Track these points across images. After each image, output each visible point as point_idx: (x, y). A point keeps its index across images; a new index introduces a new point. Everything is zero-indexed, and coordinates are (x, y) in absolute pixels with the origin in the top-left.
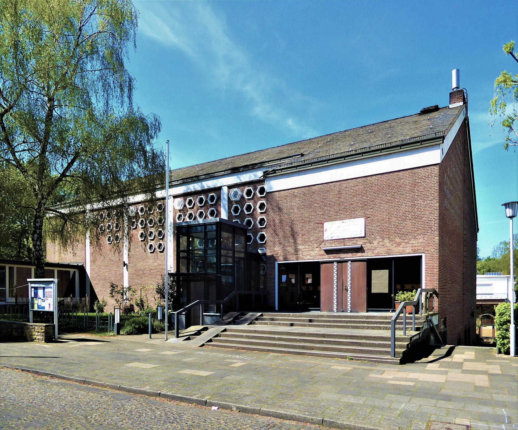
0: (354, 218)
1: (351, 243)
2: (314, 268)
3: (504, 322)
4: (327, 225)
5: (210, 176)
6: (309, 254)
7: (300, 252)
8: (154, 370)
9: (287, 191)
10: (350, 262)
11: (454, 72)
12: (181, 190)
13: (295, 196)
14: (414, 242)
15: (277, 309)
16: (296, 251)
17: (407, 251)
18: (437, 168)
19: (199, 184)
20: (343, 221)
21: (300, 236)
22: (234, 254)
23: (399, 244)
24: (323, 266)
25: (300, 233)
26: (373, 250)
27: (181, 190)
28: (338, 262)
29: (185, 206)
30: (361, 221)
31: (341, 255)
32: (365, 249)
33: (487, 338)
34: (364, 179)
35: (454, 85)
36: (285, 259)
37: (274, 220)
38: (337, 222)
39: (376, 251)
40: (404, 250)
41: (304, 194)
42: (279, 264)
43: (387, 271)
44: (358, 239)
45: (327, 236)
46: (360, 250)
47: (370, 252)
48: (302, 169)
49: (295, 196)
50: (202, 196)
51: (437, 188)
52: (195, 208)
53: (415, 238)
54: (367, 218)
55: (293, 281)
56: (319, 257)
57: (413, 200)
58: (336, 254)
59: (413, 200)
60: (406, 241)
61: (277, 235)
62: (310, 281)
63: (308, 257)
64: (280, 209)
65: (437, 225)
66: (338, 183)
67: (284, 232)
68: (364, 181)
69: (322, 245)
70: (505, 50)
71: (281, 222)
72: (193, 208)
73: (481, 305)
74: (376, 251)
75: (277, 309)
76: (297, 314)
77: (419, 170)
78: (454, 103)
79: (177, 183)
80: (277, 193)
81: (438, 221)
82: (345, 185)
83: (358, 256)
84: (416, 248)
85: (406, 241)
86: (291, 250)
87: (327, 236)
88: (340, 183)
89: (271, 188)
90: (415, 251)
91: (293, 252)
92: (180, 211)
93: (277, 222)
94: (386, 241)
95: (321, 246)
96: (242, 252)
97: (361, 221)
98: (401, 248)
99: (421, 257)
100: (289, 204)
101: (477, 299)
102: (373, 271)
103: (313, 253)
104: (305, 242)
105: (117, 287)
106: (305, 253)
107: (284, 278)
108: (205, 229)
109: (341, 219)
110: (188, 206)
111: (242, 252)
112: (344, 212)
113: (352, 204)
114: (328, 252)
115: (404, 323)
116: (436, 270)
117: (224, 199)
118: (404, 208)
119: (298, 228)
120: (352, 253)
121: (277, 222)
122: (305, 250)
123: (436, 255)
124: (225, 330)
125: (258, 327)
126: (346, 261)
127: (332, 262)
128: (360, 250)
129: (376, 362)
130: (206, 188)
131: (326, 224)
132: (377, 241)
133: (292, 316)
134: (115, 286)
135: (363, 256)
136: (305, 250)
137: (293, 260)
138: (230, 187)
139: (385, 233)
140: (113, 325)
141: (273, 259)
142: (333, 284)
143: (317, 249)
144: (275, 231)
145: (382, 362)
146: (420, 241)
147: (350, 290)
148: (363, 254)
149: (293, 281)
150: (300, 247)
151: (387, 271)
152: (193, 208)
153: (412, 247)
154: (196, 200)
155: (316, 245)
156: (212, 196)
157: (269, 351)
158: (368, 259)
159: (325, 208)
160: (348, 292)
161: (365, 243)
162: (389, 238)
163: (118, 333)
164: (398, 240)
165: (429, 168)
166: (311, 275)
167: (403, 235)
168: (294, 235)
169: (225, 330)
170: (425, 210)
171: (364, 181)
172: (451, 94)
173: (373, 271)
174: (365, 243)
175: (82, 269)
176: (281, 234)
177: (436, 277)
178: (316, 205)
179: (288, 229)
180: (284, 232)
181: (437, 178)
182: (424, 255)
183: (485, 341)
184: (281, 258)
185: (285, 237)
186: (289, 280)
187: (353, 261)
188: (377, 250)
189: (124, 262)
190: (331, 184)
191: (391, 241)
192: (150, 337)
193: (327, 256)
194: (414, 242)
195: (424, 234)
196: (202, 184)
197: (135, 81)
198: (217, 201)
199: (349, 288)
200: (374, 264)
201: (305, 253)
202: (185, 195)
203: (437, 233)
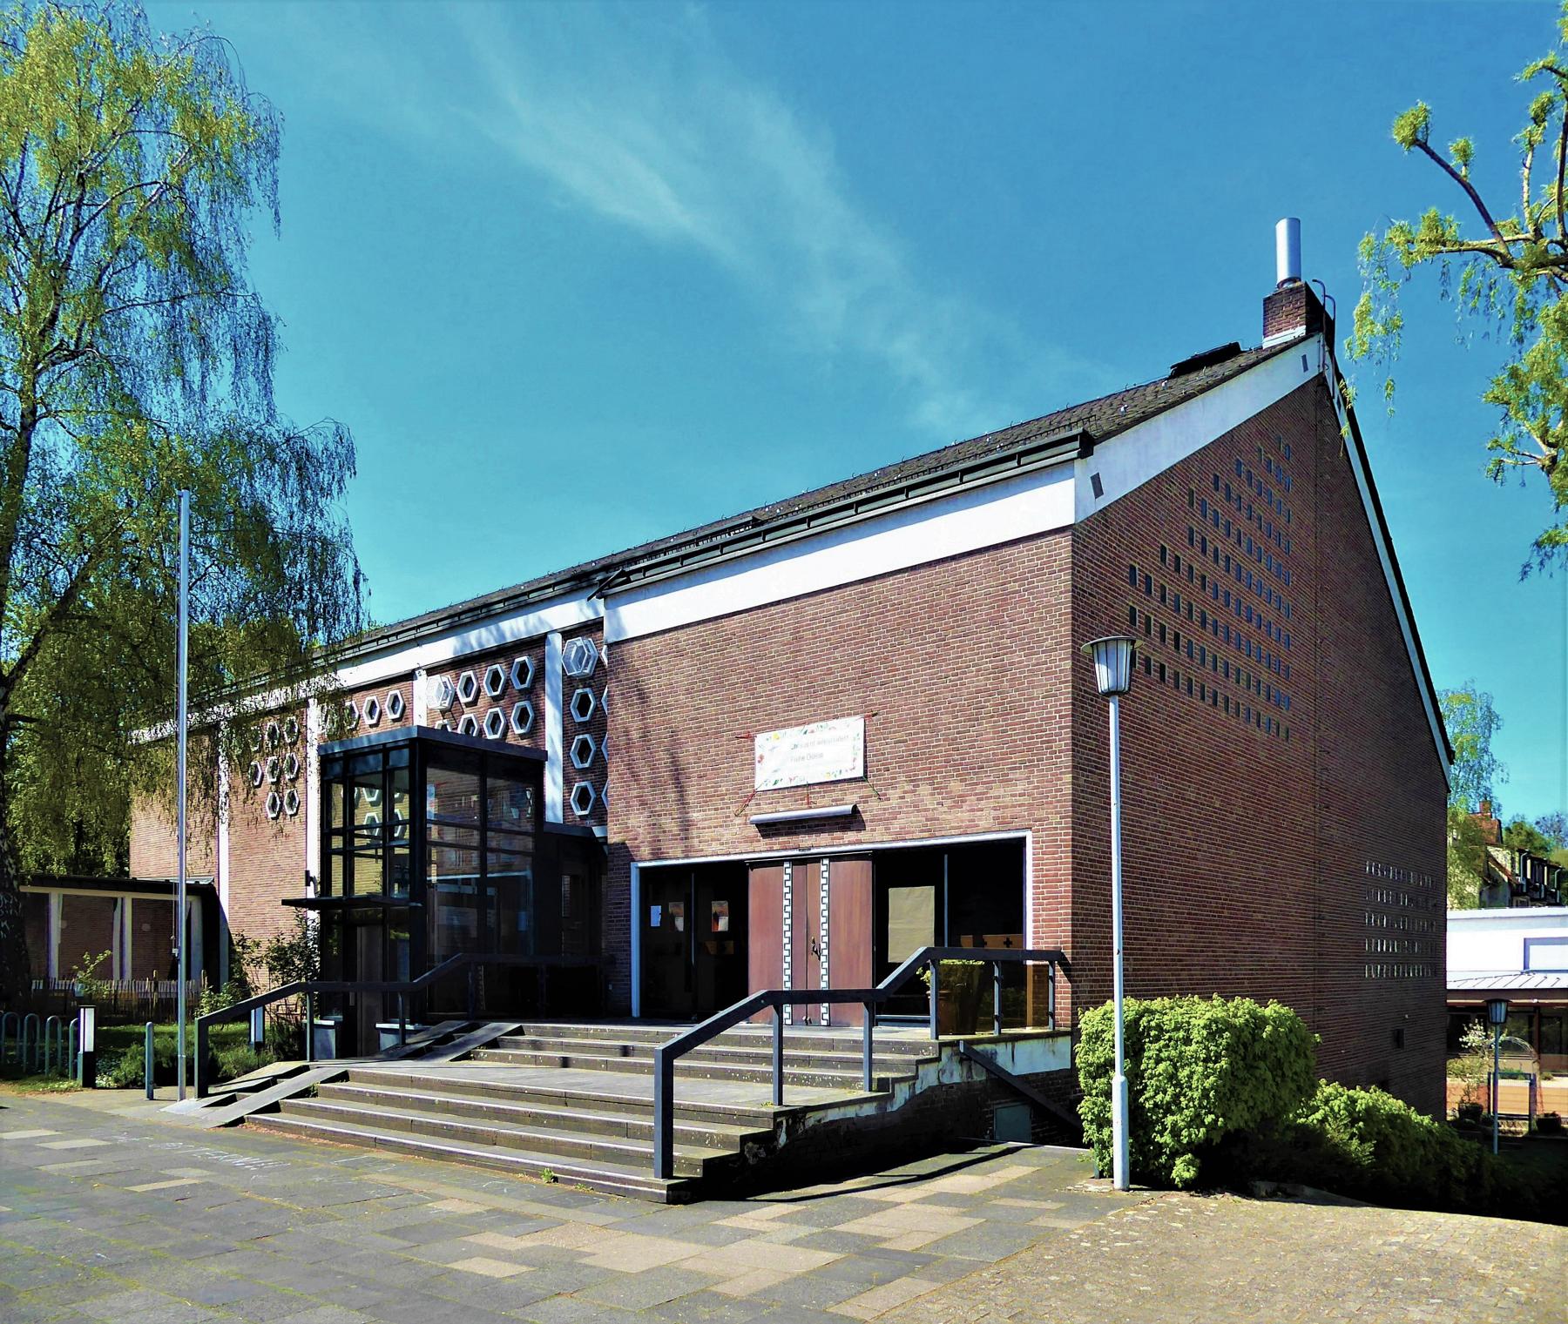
0: (836, 717)
1: (826, 800)
2: (729, 880)
3: (1099, 1066)
4: (762, 741)
5: (519, 602)
6: (720, 839)
7: (694, 832)
8: (442, 1191)
9: (660, 638)
10: (826, 861)
11: (1282, 228)
12: (445, 649)
13: (680, 654)
14: (1001, 792)
15: (635, 1012)
16: (686, 826)
17: (983, 824)
18: (1065, 541)
19: (492, 627)
20: (807, 727)
21: (694, 781)
22: (483, 840)
23: (959, 801)
24: (755, 876)
25: (694, 769)
26: (886, 820)
27: (445, 649)
28: (797, 861)
29: (456, 698)
30: (850, 729)
31: (801, 837)
32: (865, 817)
33: (1510, 1118)
34: (862, 587)
35: (1283, 273)
36: (657, 855)
37: (627, 732)
38: (788, 731)
39: (896, 826)
40: (967, 822)
41: (704, 646)
42: (642, 870)
43: (930, 890)
44: (846, 785)
45: (764, 779)
46: (852, 821)
47: (880, 829)
48: (695, 566)
49: (680, 654)
50: (497, 666)
51: (1066, 608)
52: (481, 702)
53: (1005, 781)
54: (870, 716)
55: (680, 924)
56: (743, 847)
57: (999, 650)
58: (787, 834)
59: (999, 650)
60: (979, 789)
61: (635, 776)
62: (723, 924)
63: (715, 846)
64: (643, 697)
65: (1067, 734)
66: (792, 606)
67: (653, 768)
68: (863, 596)
69: (752, 808)
70: (1400, 131)
71: (645, 736)
72: (474, 703)
73: (1537, 1006)
74: (896, 826)
75: (635, 1012)
76: (607, 1027)
77: (1014, 550)
78: (1279, 330)
79: (434, 629)
80: (635, 645)
81: (1067, 722)
82: (810, 611)
83: (848, 841)
84: (1009, 813)
85: (979, 789)
86: (670, 824)
87: (764, 779)
88: (797, 604)
89: (619, 629)
90: (1003, 824)
91: (675, 830)
92: (443, 712)
93: (635, 735)
94: (925, 789)
95: (747, 810)
96: (525, 833)
97: (850, 729)
98: (963, 815)
99: (1021, 842)
100: (664, 681)
101: (1449, 986)
102: (891, 891)
103: (727, 834)
104: (706, 799)
105: (258, 945)
106: (707, 835)
107: (656, 911)
108: (386, 760)
109: (801, 722)
110: (463, 700)
111: (525, 833)
112: (805, 703)
113: (830, 672)
114: (768, 829)
115: (866, 1065)
116: (1065, 887)
117: (554, 671)
118: (973, 681)
119: (687, 756)
120: (831, 831)
121: (635, 735)
122: (706, 824)
123: (1066, 836)
124: (344, 1077)
125: (486, 1070)
126: (817, 859)
127: (778, 862)
128: (852, 821)
129: (617, 1191)
130: (509, 639)
131: (760, 739)
132: (899, 792)
133: (594, 1037)
134: (248, 943)
135: (860, 842)
136: (706, 824)
137: (675, 857)
138: (567, 634)
139: (921, 765)
140: (76, 1056)
141: (624, 853)
142: (781, 933)
143: (738, 821)
144: (630, 766)
145: (626, 1193)
146: (1020, 788)
147: (825, 952)
148: (862, 835)
149: (680, 924)
150: (695, 816)
151: (930, 890)
152: (474, 703)
153: (995, 809)
154: (481, 677)
155: (733, 808)
156: (523, 665)
157: (378, 1143)
158: (875, 851)
159: (760, 688)
160: (823, 959)
161: (865, 799)
162: (931, 781)
163: (89, 1083)
164: (956, 786)
165: (1042, 542)
166: (725, 904)
167: (969, 770)
168: (678, 776)
169: (344, 1077)
170: (1032, 685)
171: (863, 596)
172: (1267, 301)
173: (891, 891)
174: (865, 799)
175: (206, 895)
176: (645, 773)
177: (1065, 910)
178: (734, 679)
179: (663, 756)
180: (653, 768)
181: (1066, 577)
182: (1029, 835)
183: (1504, 1127)
184: (645, 851)
185: (655, 783)
186: (668, 918)
187: (835, 858)
188: (901, 823)
189: (307, 873)
190: (773, 610)
191: (938, 789)
192: (150, 1096)
193: (763, 843)
194: (1001, 792)
195: (1030, 767)
196: (498, 629)
197: (280, 326)
198: (534, 681)
199: (823, 946)
200: (894, 868)
201: (707, 835)
202: (457, 664)
203: (1066, 760)
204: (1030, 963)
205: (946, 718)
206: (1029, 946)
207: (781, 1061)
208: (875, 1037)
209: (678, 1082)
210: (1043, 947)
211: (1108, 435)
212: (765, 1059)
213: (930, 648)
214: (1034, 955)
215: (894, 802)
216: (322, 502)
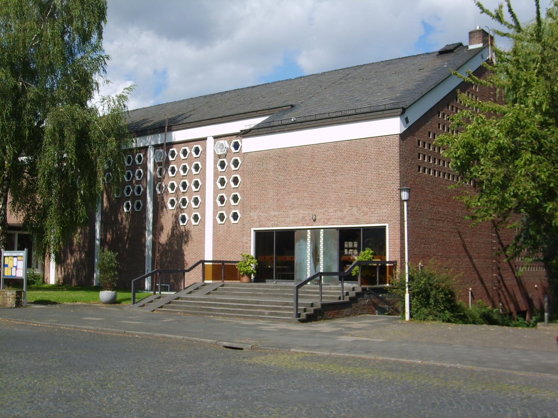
60: (372, 210)
85: (372, 210)
94: (355, 209)
99: (384, 228)
122: (280, 216)
132: (346, 210)
146: (385, 210)
164: (365, 209)
172: (470, 33)
181: (398, 148)
182: (387, 225)
194: (379, 212)
204: (388, 265)
205: (361, 188)
206: (387, 260)
207: (322, 293)
208: (308, 231)
209: (299, 299)
210: (392, 260)
211: (407, 108)
212: (317, 293)
213: (357, 165)
214: (389, 262)
215: (345, 213)
216: (126, 103)
